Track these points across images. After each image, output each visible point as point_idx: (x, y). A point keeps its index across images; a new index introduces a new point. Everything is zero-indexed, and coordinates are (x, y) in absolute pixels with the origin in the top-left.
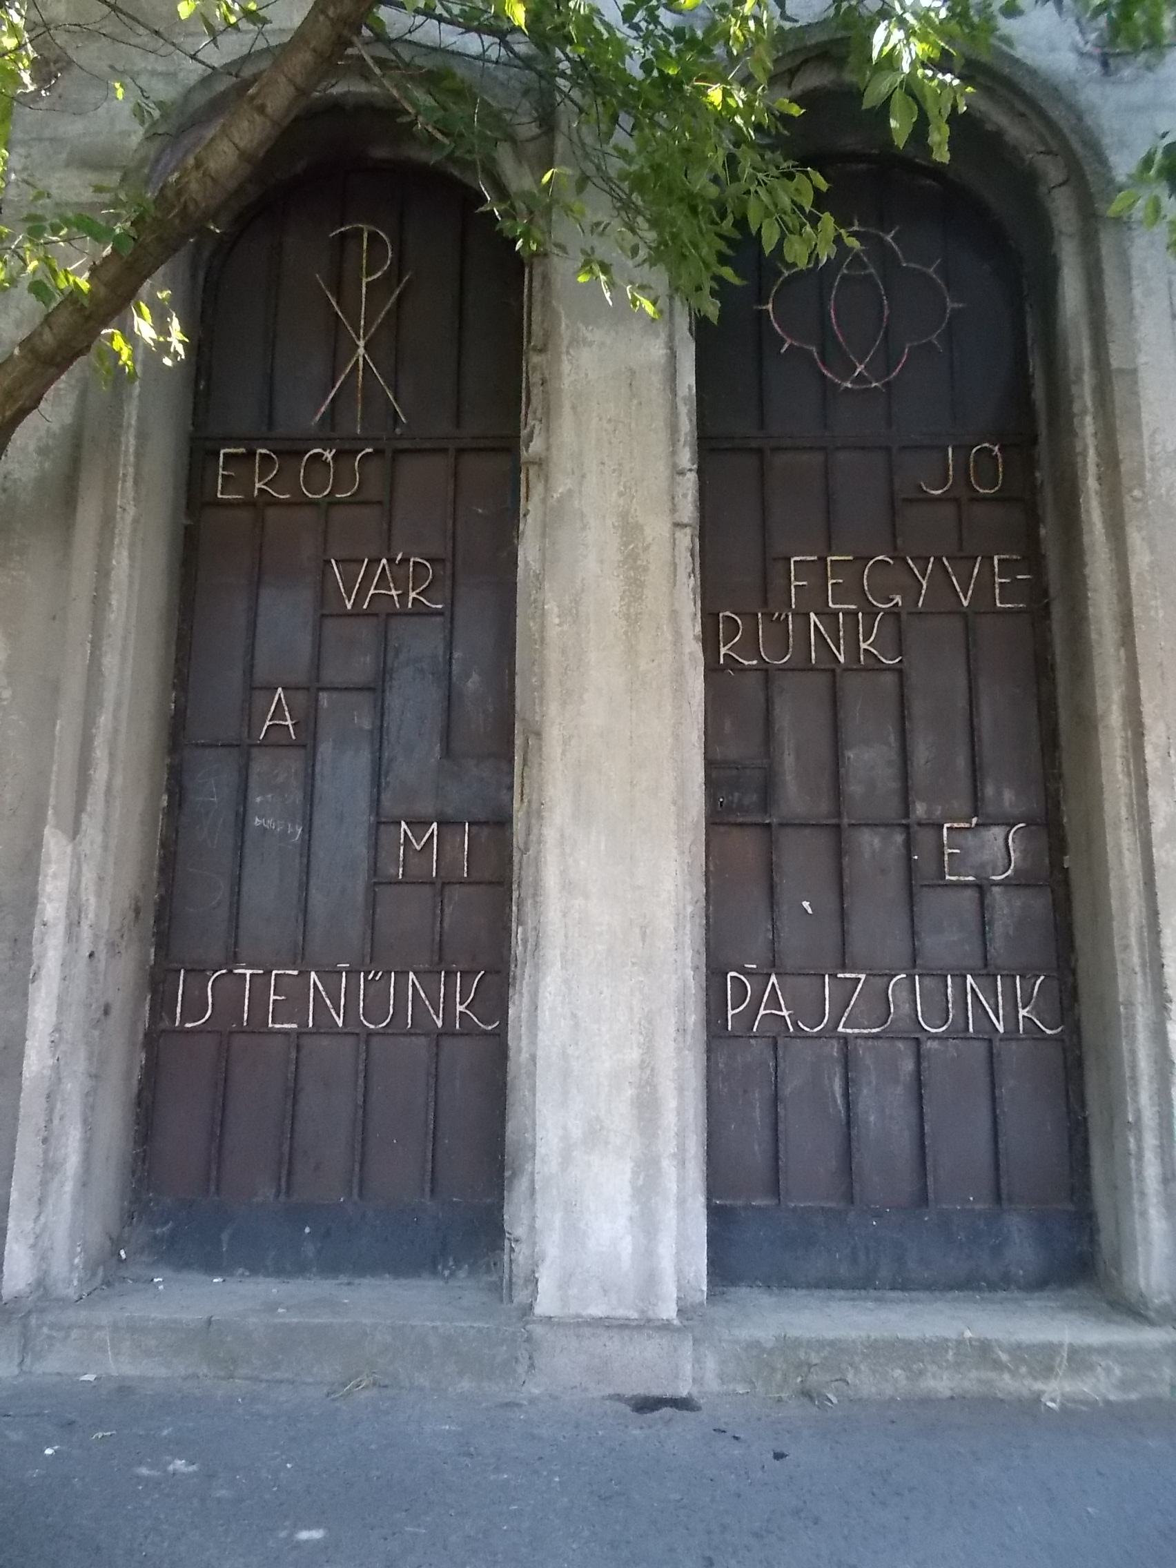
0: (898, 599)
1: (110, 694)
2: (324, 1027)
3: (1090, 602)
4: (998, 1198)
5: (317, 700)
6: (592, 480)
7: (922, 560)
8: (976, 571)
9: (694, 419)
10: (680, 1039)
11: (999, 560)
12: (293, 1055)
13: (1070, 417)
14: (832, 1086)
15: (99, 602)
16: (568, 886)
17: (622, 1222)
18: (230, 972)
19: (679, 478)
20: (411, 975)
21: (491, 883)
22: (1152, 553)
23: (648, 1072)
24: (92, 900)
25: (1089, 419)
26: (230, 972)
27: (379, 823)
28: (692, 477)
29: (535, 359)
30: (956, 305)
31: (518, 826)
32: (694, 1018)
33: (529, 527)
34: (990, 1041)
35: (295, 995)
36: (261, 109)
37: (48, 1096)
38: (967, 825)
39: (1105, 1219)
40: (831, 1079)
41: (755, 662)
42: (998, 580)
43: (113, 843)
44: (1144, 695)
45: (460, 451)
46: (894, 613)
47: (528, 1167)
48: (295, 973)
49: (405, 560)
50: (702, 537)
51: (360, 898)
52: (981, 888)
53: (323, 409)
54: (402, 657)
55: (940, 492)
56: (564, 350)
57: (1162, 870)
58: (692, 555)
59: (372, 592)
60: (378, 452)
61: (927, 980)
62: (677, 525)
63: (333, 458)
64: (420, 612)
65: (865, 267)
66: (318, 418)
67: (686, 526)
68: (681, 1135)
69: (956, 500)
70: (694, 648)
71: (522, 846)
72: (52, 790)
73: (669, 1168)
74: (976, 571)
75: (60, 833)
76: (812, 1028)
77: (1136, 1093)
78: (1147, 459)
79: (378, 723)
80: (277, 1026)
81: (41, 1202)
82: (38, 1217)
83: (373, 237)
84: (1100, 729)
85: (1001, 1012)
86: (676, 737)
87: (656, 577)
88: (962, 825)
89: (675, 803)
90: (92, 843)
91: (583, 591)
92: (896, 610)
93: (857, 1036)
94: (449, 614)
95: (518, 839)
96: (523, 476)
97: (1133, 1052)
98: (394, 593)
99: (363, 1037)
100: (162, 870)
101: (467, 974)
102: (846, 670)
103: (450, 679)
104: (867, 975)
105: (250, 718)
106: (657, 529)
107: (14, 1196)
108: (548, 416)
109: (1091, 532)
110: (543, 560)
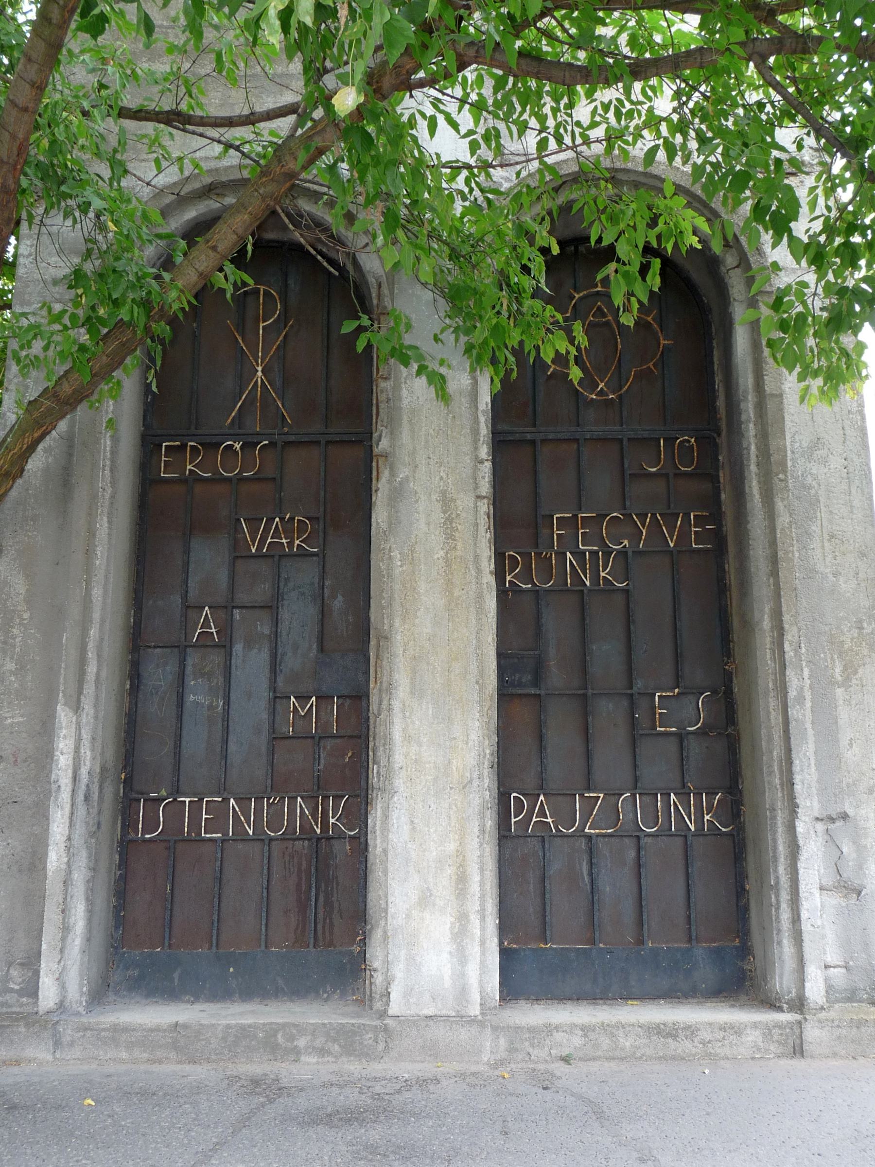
0: (626, 542)
1: (96, 616)
2: (241, 837)
3: (751, 547)
4: (690, 940)
5: (232, 615)
6: (423, 469)
7: (643, 516)
8: (679, 523)
9: (490, 426)
10: (481, 837)
11: (694, 516)
12: (219, 855)
13: (740, 423)
14: (581, 869)
15: (89, 553)
16: (408, 739)
17: (445, 956)
18: (175, 800)
19: (479, 466)
20: (299, 799)
21: (351, 737)
22: (791, 516)
23: (461, 858)
24: (88, 753)
25: (751, 425)
26: (175, 800)
27: (276, 697)
28: (488, 465)
29: (383, 384)
30: (666, 342)
31: (374, 699)
32: (490, 823)
33: (380, 500)
34: (686, 836)
35: (220, 813)
36: (214, 248)
37: (65, 882)
38: (671, 694)
39: (758, 951)
40: (581, 865)
41: (530, 586)
42: (693, 529)
43: (101, 714)
44: (784, 609)
45: (328, 443)
46: (623, 553)
47: (382, 923)
48: (220, 799)
49: (292, 519)
50: (494, 504)
51: (264, 749)
52: (681, 737)
53: (233, 414)
54: (291, 585)
55: (654, 469)
56: (403, 380)
57: (794, 722)
58: (488, 517)
59: (269, 540)
60: (272, 444)
61: (644, 798)
62: (479, 497)
63: (241, 448)
64: (303, 554)
65: (604, 315)
66: (229, 421)
67: (484, 497)
68: (482, 898)
69: (666, 475)
70: (490, 580)
71: (376, 712)
72: (62, 680)
73: (475, 920)
74: (679, 523)
75: (68, 709)
76: (568, 830)
77: (776, 867)
78: (789, 452)
79: (274, 629)
80: (208, 836)
81: (62, 951)
82: (59, 962)
83: (266, 293)
84: (756, 631)
85: (693, 817)
86: (478, 639)
87: (463, 528)
88: (668, 694)
89: (477, 683)
90: (87, 715)
91: (416, 543)
92: (624, 550)
93: (598, 835)
94: (322, 556)
95: (374, 707)
96: (374, 464)
97: (775, 841)
98: (284, 541)
99: (267, 842)
100: (127, 732)
101: (338, 798)
102: (590, 590)
103: (323, 599)
104: (605, 794)
105: (186, 626)
106: (464, 502)
107: (44, 947)
108: (394, 425)
109: (752, 501)
110: (390, 524)
